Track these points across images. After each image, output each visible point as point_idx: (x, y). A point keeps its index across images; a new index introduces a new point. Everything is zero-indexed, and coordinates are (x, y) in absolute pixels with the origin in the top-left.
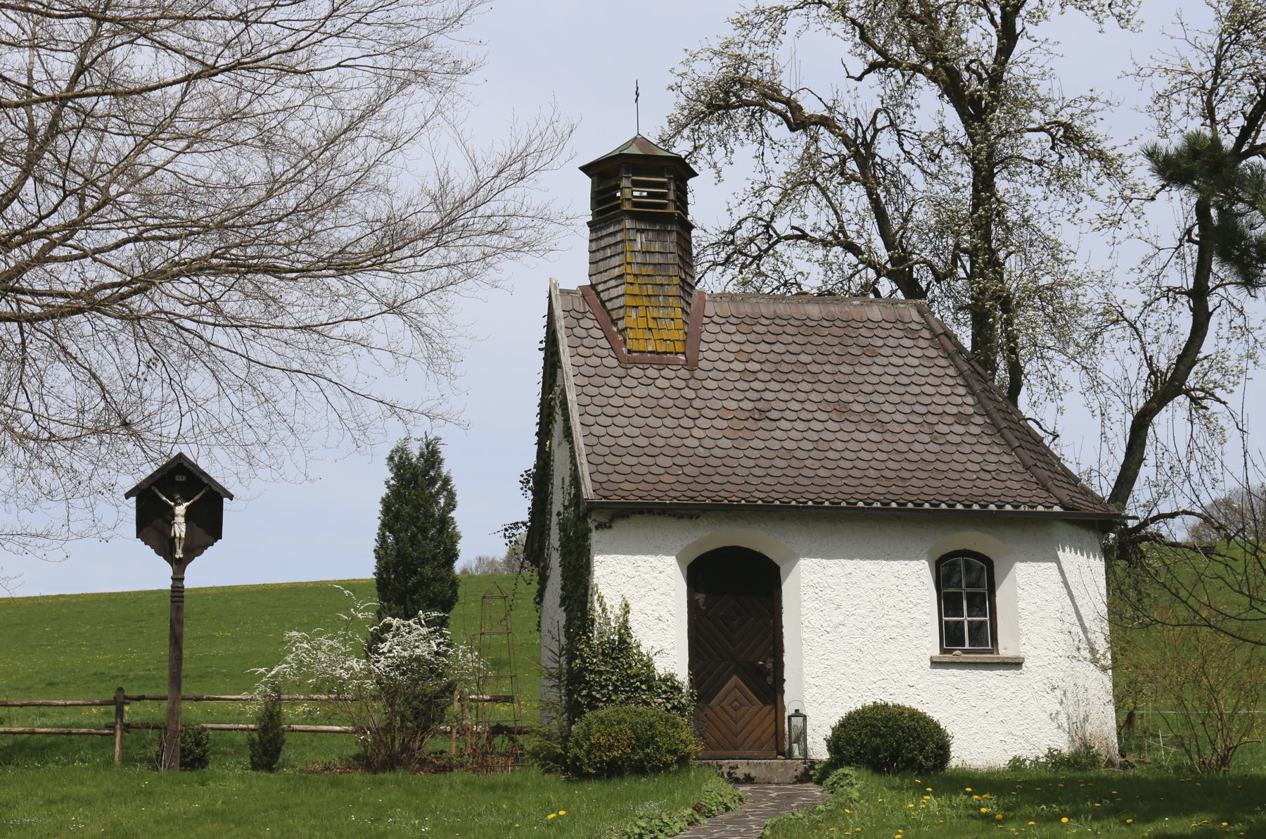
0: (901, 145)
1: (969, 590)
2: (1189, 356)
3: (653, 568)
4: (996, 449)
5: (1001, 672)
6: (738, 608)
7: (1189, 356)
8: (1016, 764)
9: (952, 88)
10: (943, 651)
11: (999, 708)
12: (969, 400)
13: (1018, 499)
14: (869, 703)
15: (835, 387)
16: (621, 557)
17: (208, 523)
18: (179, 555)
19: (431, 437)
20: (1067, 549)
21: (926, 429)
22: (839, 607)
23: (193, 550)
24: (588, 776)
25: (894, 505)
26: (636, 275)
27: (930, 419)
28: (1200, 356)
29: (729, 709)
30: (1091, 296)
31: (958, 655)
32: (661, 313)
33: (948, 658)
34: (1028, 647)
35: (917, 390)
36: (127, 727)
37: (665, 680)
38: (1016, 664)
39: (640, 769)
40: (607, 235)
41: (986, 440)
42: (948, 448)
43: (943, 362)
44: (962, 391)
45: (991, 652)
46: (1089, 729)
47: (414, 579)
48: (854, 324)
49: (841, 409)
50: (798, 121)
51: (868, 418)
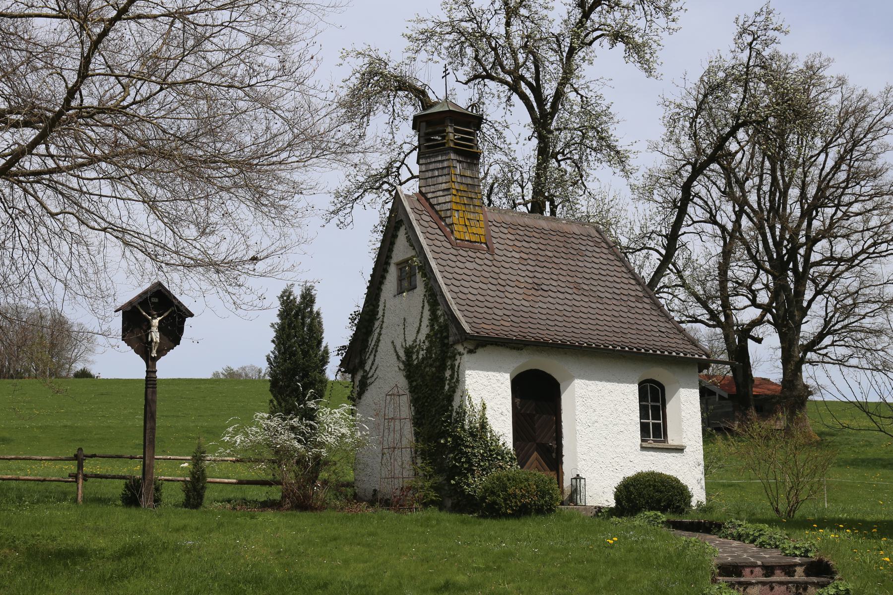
1: (658, 404)
3: (498, 380)
16: (481, 372)
17: (173, 334)
18: (154, 354)
19: (308, 284)
23: (162, 352)
24: (507, 516)
26: (457, 190)
34: (686, 440)
36: (86, 477)
38: (680, 450)
40: (435, 162)
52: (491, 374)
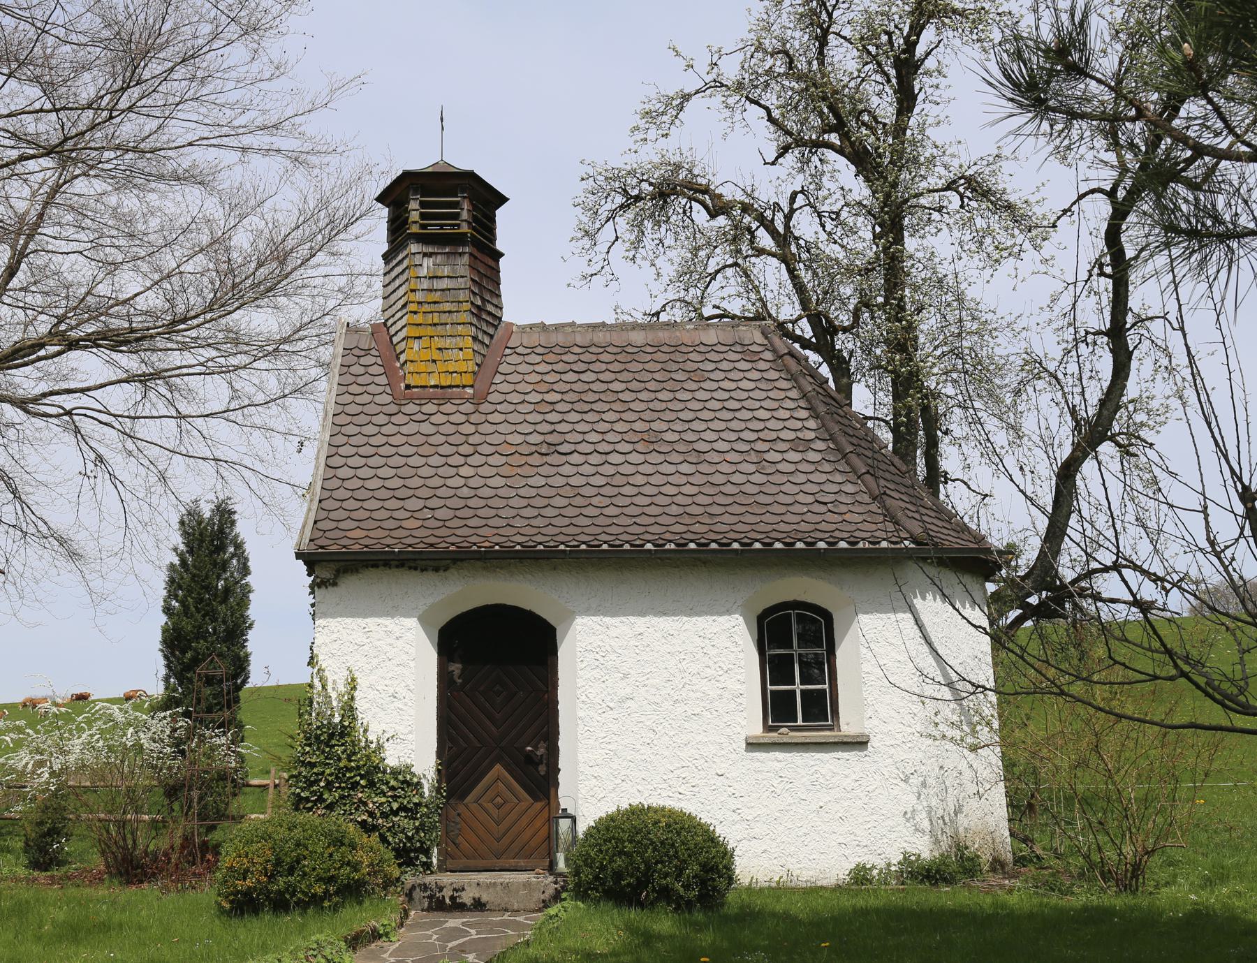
0: (823, 226)
2: (1112, 398)
3: (389, 633)
4: (838, 478)
5: (846, 755)
6: (501, 680)
7: (1112, 398)
8: (861, 876)
9: (861, 159)
10: (767, 728)
11: (837, 801)
12: (812, 424)
13: (857, 534)
14: (625, 806)
15: (647, 415)
16: (348, 620)
19: (221, 497)
20: (929, 597)
21: (753, 457)
22: (626, 676)
25: (692, 546)
27: (760, 446)
28: (1124, 399)
29: (489, 806)
30: (1004, 347)
31: (785, 734)
32: (448, 342)
33: (773, 736)
34: (875, 721)
35: (748, 415)
37: (395, 773)
38: (859, 744)
39: (280, 905)
40: (397, 265)
41: (827, 467)
42: (777, 478)
43: (784, 384)
44: (803, 414)
45: (831, 728)
46: (963, 821)
47: (189, 655)
48: (683, 349)
49: (651, 440)
50: (718, 208)
51: (681, 447)
52: (371, 622)
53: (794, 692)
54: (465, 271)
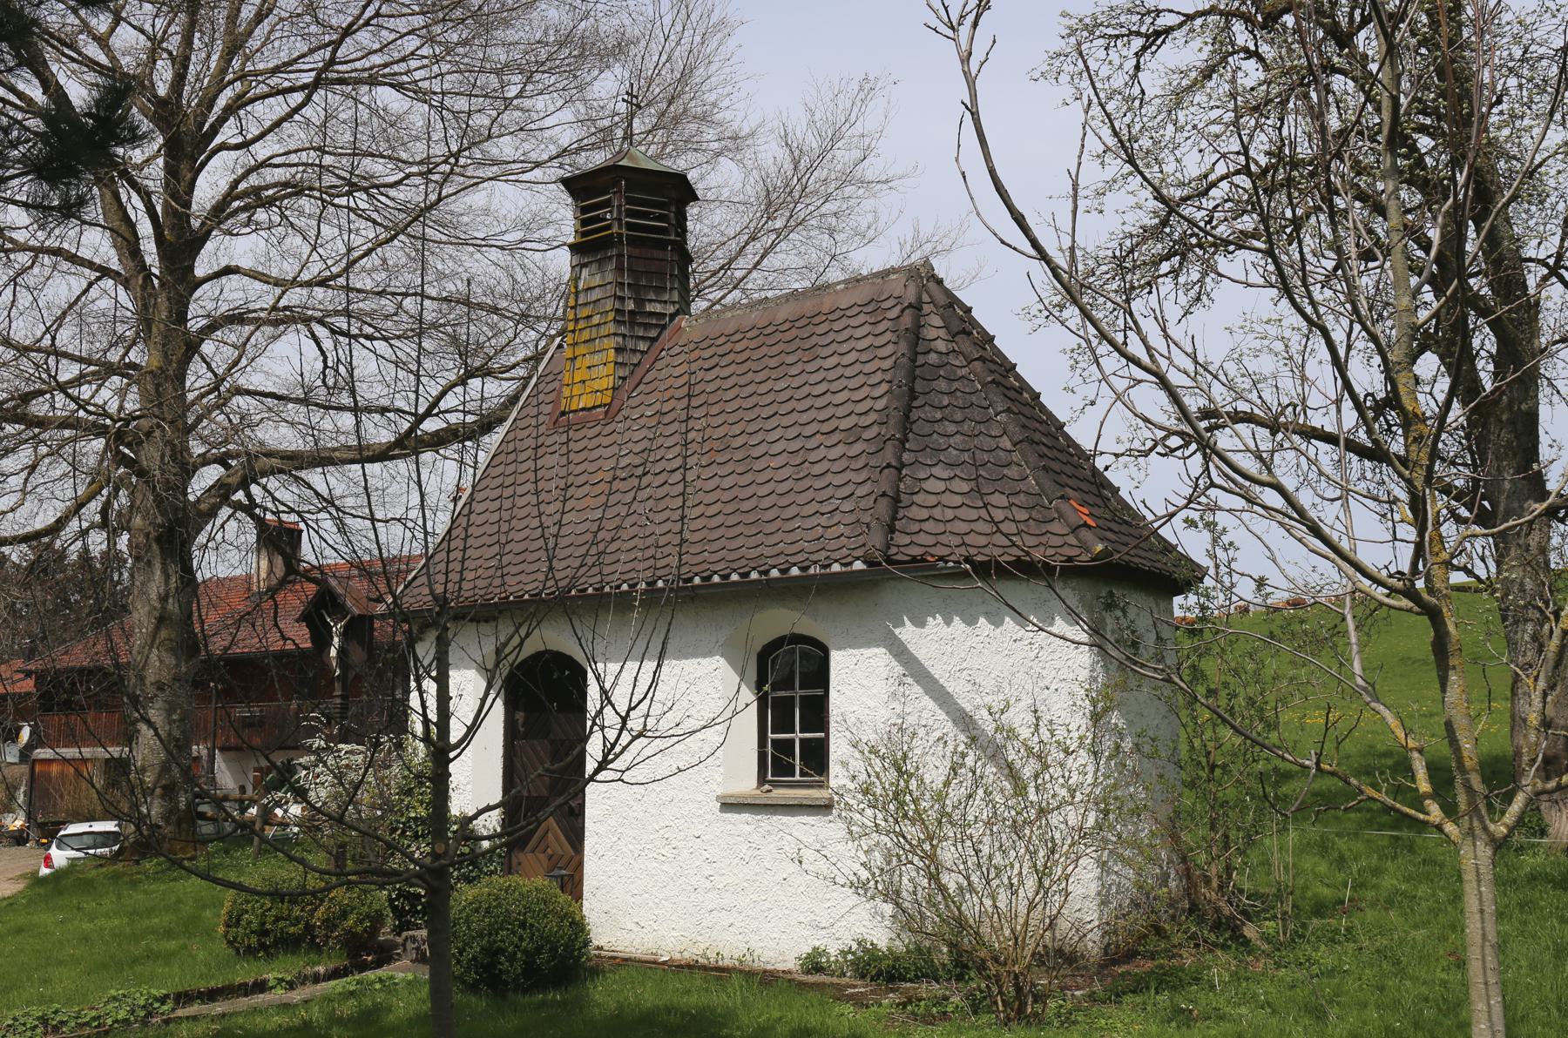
5: (785, 819)
53: (793, 741)
54: (610, 277)
